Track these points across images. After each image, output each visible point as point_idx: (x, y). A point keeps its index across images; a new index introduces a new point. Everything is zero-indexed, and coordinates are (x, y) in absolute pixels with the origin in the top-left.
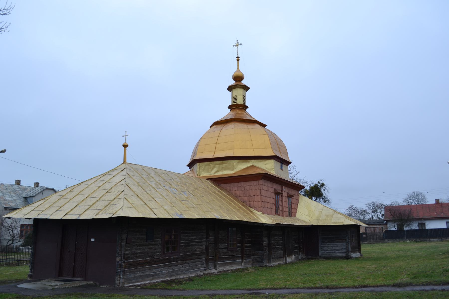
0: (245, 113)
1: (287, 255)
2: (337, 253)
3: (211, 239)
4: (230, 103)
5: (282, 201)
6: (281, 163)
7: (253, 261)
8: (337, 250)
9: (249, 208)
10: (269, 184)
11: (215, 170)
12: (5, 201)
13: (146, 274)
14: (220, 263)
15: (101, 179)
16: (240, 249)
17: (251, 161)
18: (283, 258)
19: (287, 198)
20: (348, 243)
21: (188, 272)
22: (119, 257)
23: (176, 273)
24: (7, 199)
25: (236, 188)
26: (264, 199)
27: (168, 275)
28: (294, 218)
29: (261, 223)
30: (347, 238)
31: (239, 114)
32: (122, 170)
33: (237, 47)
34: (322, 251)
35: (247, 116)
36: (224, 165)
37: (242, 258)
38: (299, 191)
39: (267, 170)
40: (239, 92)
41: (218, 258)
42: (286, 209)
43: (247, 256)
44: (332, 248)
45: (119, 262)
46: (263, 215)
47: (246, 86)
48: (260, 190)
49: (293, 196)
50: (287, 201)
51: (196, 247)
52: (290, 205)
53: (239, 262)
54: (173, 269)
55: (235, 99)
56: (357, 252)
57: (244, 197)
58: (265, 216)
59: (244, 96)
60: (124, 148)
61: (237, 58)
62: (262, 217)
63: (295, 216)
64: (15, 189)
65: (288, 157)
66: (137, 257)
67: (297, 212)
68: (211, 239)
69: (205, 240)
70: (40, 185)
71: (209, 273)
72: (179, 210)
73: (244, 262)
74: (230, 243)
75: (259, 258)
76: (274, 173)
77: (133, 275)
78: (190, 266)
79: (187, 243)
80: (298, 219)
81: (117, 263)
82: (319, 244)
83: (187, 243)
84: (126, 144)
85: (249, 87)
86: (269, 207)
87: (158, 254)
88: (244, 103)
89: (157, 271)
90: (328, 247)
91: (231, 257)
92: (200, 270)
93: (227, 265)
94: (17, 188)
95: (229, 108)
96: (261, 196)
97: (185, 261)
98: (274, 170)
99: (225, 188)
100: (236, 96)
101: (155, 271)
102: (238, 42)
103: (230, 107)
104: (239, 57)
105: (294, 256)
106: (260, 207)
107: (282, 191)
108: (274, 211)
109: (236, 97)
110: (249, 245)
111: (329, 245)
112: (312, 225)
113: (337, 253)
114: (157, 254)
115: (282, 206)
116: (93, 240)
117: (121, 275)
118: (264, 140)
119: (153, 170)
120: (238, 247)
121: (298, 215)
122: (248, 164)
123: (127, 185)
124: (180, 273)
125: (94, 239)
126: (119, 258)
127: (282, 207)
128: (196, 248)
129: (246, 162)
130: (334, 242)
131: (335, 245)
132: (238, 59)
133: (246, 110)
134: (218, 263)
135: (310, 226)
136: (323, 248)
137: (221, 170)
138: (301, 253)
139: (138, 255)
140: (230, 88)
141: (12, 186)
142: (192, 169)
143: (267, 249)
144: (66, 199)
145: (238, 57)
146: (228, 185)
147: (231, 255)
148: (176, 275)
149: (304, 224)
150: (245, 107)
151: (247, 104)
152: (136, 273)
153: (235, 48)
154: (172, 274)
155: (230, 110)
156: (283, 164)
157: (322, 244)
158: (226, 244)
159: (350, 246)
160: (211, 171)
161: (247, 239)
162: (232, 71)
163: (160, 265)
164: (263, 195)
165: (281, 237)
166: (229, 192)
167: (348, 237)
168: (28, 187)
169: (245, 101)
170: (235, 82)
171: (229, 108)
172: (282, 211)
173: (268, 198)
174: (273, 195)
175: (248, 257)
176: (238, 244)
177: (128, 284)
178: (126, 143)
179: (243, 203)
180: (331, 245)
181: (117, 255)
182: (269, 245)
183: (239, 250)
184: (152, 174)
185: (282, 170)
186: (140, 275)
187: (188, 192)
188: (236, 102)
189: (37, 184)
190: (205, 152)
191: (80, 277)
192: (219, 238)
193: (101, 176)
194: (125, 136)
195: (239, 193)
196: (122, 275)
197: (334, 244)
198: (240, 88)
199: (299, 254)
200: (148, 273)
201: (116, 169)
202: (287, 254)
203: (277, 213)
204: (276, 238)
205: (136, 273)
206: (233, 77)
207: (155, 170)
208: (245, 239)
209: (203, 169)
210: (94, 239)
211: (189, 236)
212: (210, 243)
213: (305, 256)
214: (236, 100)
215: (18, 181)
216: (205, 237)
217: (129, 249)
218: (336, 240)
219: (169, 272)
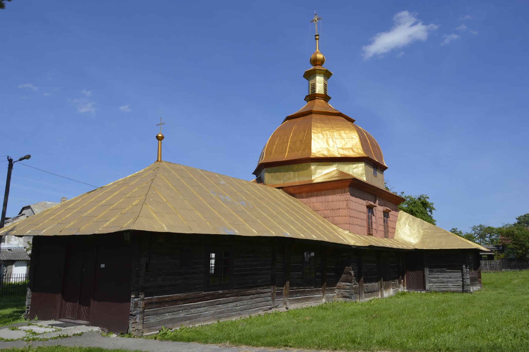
1: (383, 288)
2: (451, 287)
7: (338, 296)
8: (451, 282)
13: (179, 316)
14: (292, 299)
16: (320, 279)
19: (382, 213)
21: (244, 312)
23: (226, 315)
27: (215, 317)
29: (349, 245)
34: (429, 283)
38: (397, 205)
41: (289, 291)
44: (444, 279)
47: (327, 71)
53: (319, 297)
54: (223, 308)
56: (478, 285)
59: (325, 83)
60: (158, 140)
63: (393, 238)
69: (270, 267)
71: (412, 214)
73: (325, 298)
76: (365, 180)
77: (159, 318)
82: (426, 275)
88: (325, 93)
89: (198, 312)
90: (438, 278)
91: (307, 290)
92: (263, 309)
93: (302, 302)
95: (305, 100)
97: (240, 297)
101: (194, 312)
105: (392, 289)
110: (332, 274)
112: (416, 249)
114: (197, 286)
116: (103, 266)
124: (233, 313)
125: (101, 267)
128: (256, 279)
130: (446, 272)
131: (448, 276)
134: (289, 298)
135: (413, 250)
138: (401, 285)
148: (226, 317)
149: (405, 247)
152: (164, 315)
154: (220, 315)
156: (376, 168)
157: (429, 275)
158: (301, 273)
159: (469, 278)
161: (329, 267)
163: (202, 303)
165: (375, 265)
169: (326, 92)
173: (357, 212)
174: (365, 209)
176: (317, 273)
177: (150, 332)
179: (324, 219)
180: (442, 276)
181: (132, 289)
183: (318, 281)
186: (169, 317)
190: (338, 225)
192: (291, 264)
195: (318, 205)
196: (139, 318)
198: (320, 74)
199: (399, 287)
200: (182, 315)
202: (383, 287)
203: (370, 234)
208: (328, 266)
212: (277, 272)
213: (407, 289)
217: (151, 279)
219: (215, 313)
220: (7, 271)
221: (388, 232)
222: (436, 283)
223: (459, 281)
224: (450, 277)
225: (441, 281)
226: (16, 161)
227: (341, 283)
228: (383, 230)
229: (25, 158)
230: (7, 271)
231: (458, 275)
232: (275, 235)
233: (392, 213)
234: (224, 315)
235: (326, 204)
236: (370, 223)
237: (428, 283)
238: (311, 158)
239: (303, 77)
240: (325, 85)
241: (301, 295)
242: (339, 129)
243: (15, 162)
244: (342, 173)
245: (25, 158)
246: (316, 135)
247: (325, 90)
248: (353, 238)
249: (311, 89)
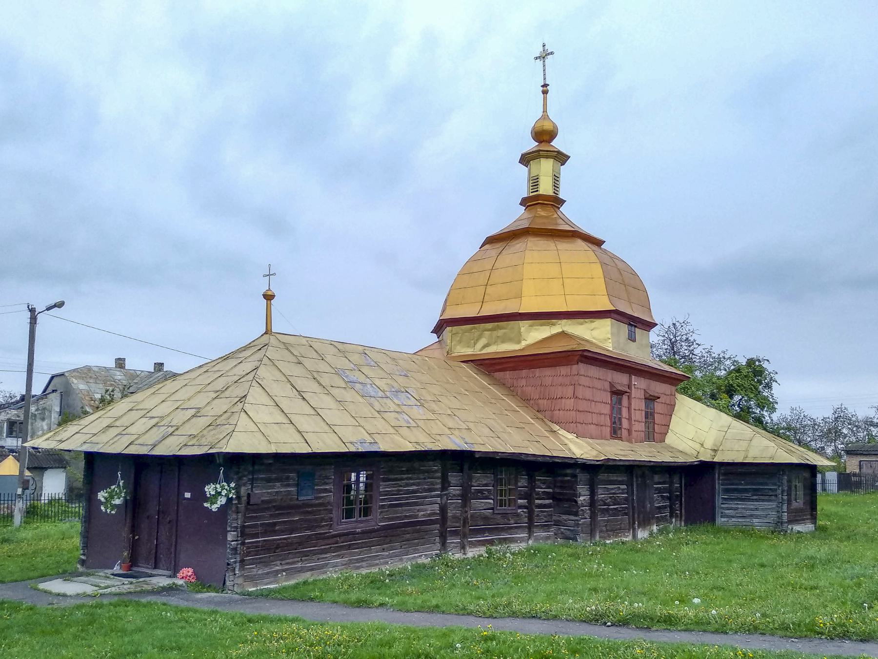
0: (556, 216)
1: (636, 525)
3: (454, 490)
4: (524, 192)
5: (628, 408)
6: (630, 324)
8: (757, 517)
9: (550, 423)
10: (594, 371)
11: (483, 342)
12: (92, 400)
15: (215, 369)
17: (560, 322)
18: (629, 530)
20: (781, 503)
21: (396, 560)
22: (232, 533)
24: (96, 397)
25: (524, 379)
26: (583, 405)
28: (659, 445)
30: (779, 491)
31: (542, 217)
32: (260, 349)
33: (544, 61)
34: (722, 517)
35: (560, 221)
36: (500, 333)
37: (530, 529)
39: (594, 341)
40: (546, 166)
42: (641, 427)
43: (540, 525)
45: (233, 543)
46: (577, 440)
47: (559, 152)
48: (572, 387)
49: (659, 398)
50: (644, 408)
51: (418, 508)
52: (649, 415)
55: (535, 182)
57: (540, 401)
58: (582, 442)
59: (555, 175)
60: (266, 300)
61: (543, 86)
62: (575, 443)
64: (112, 376)
65: (651, 312)
67: (669, 431)
68: (454, 490)
72: (369, 434)
74: (499, 498)
75: (569, 530)
78: (401, 547)
79: (396, 499)
80: (670, 449)
81: (228, 546)
83: (396, 499)
84: (269, 293)
85: (567, 156)
86: (595, 421)
87: (327, 525)
90: (737, 509)
94: (119, 375)
95: (521, 204)
96: (576, 400)
98: (610, 341)
99: (501, 381)
100: (536, 178)
102: (546, 48)
103: (524, 202)
104: (548, 85)
106: (572, 422)
107: (629, 387)
108: (607, 431)
109: (538, 178)
110: (547, 502)
111: (739, 506)
113: (756, 524)
115: (628, 419)
116: (188, 495)
117: (237, 569)
118: (592, 276)
119: (335, 346)
120: (520, 507)
121: (670, 439)
122: (552, 328)
123: (257, 381)
126: (231, 534)
127: (629, 424)
129: (548, 325)
130: (749, 500)
131: (752, 507)
132: (545, 88)
133: (559, 208)
134: (469, 540)
136: (724, 511)
137: (495, 343)
139: (277, 528)
140: (526, 159)
141: (107, 370)
143: (588, 511)
144: (142, 410)
145: (545, 85)
146: (508, 374)
147: (502, 523)
148: (367, 566)
149: (681, 459)
150: (556, 202)
151: (561, 196)
153: (539, 63)
154: (357, 565)
155: (524, 208)
158: (491, 501)
160: (475, 344)
161: (543, 490)
162: (531, 118)
164: (581, 397)
165: (625, 487)
166: (511, 390)
167: (783, 491)
168: (140, 372)
170: (537, 144)
171: (521, 204)
172: (629, 431)
174: (607, 397)
175: (546, 527)
176: (520, 501)
178: (269, 290)
181: (229, 529)
182: (592, 503)
184: (330, 354)
185: (634, 341)
187: (407, 392)
188: (537, 191)
193: (218, 361)
194: (268, 275)
196: (239, 569)
197: (751, 505)
198: (547, 157)
201: (251, 345)
202: (636, 523)
203: (615, 433)
205: (272, 563)
206: (534, 134)
207: (340, 346)
209: (459, 341)
210: (190, 494)
211: (401, 486)
212: (449, 500)
214: (538, 185)
215: (119, 359)
216: (439, 486)
218: (753, 496)
220: (36, 488)
222: (733, 517)
223: (769, 514)
224: (756, 509)
225: (741, 515)
226: (42, 312)
227: (561, 517)
228: (644, 430)
229: (55, 306)
230: (36, 488)
231: (769, 505)
234: (364, 564)
235: (542, 390)
237: (720, 517)
238: (520, 313)
241: (490, 534)
243: (40, 313)
245: (55, 306)
248: (580, 447)
249: (532, 186)
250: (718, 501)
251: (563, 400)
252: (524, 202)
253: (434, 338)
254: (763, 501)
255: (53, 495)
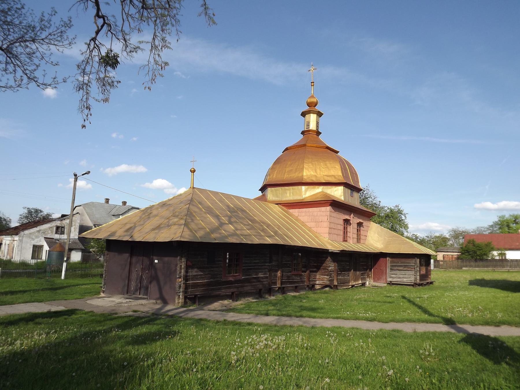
6: (351, 189)
30: (416, 267)
47: (319, 112)
66: (197, 279)
70: (127, 204)
74: (294, 267)
87: (219, 277)
116: (156, 261)
131: (404, 273)
142: (264, 193)
165: (348, 263)
174: (342, 222)
189: (124, 203)
191: (13, 273)
198: (314, 113)
203: (345, 240)
204: (343, 264)
215: (107, 199)
221: (360, 239)
222: (395, 278)
231: (410, 273)
232: (272, 243)
233: (365, 223)
236: (345, 232)
239: (301, 115)
240: (318, 123)
242: (325, 160)
244: (326, 195)
246: (307, 164)
247: (317, 126)
250: (388, 270)
251: (322, 223)
252: (303, 133)
253: (260, 194)
254: (409, 270)
255: (28, 261)
